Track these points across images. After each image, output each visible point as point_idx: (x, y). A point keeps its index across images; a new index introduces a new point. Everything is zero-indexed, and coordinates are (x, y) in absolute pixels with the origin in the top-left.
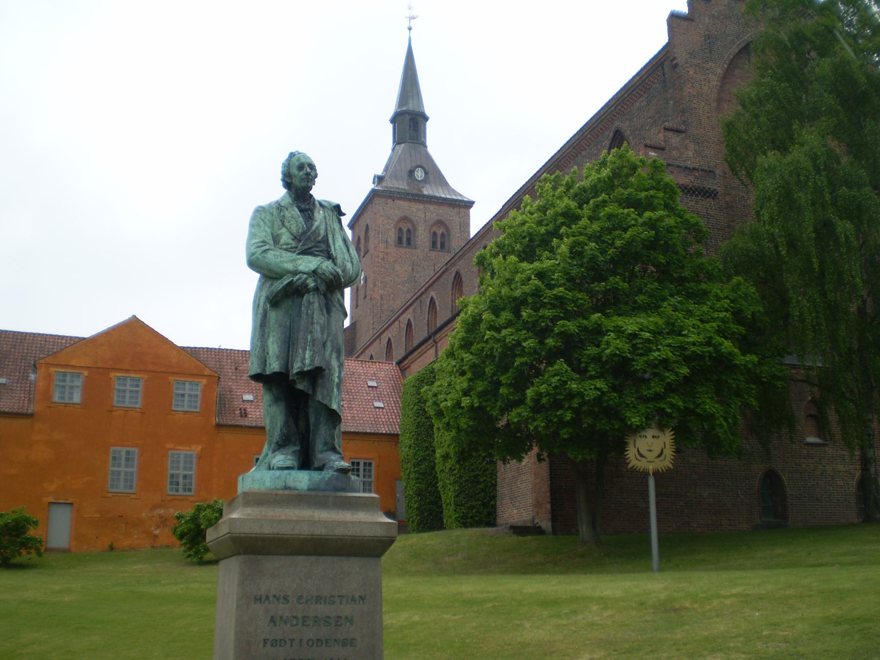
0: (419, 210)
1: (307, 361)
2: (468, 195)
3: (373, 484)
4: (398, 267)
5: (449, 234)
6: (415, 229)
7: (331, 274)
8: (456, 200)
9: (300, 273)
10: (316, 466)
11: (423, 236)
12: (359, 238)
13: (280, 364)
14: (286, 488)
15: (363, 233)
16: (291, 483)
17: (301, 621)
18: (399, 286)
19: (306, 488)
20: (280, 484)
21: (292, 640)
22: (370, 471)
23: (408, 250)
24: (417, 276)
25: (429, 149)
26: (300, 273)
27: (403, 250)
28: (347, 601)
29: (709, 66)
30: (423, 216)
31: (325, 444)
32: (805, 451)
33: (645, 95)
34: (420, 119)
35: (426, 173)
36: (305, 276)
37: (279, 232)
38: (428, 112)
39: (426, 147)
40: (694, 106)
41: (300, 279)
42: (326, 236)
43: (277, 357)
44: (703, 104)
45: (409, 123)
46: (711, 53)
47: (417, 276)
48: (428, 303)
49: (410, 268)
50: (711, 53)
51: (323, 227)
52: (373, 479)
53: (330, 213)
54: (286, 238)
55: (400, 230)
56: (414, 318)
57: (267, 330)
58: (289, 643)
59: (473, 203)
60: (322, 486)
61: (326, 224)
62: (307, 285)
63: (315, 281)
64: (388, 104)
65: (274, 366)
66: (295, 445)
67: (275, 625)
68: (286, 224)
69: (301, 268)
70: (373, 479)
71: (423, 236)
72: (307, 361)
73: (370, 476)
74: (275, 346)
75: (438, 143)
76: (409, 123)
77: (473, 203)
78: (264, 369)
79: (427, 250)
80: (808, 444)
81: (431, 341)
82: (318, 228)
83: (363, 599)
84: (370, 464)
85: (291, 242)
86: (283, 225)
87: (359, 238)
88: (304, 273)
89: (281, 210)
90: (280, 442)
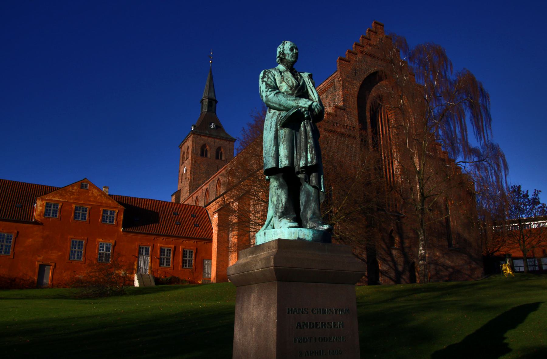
1: (309, 160)
4: (201, 166)
74: (286, 151)
84: (192, 252)
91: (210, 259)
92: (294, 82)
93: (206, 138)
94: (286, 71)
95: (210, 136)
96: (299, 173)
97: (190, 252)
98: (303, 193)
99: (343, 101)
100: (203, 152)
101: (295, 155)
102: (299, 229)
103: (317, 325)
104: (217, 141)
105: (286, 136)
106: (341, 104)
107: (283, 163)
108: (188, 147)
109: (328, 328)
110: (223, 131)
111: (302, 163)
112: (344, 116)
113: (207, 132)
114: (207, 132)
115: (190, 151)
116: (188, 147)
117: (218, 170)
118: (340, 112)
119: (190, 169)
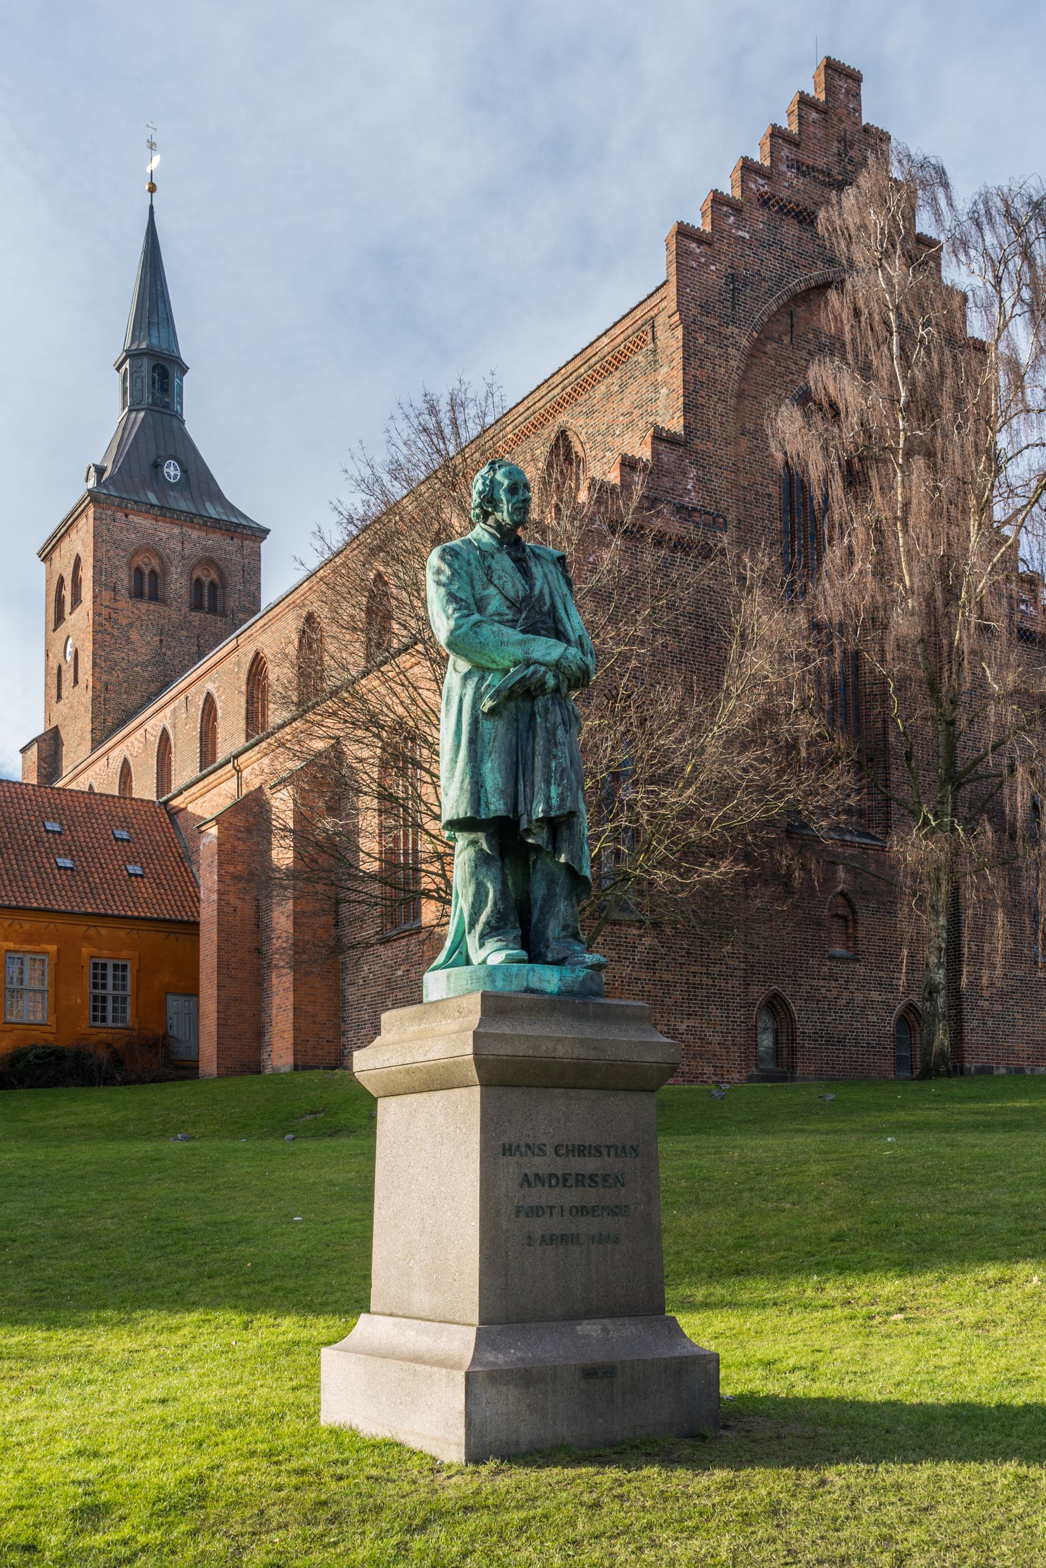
0: (171, 536)
1: (554, 802)
2: (257, 515)
3: (129, 1000)
4: (134, 636)
5: (224, 587)
6: (165, 571)
7: (579, 668)
8: (238, 525)
9: (533, 663)
10: (550, 957)
11: (177, 584)
12: (61, 580)
13: (505, 804)
14: (529, 990)
15: (70, 570)
16: (535, 984)
17: (561, 1179)
18: (138, 669)
19: (556, 990)
20: (516, 985)
21: (551, 1208)
22: (124, 978)
23: (152, 607)
24: (169, 653)
25: (187, 426)
26: (535, 662)
27: (144, 606)
28: (616, 1152)
29: (728, 331)
30: (179, 548)
31: (565, 927)
32: (825, 969)
33: (617, 374)
34: (174, 372)
35: (184, 471)
36: (543, 668)
37: (486, 592)
38: (186, 354)
39: (183, 422)
40: (701, 401)
41: (535, 672)
42: (553, 605)
43: (502, 792)
44: (715, 398)
45: (155, 371)
46: (734, 308)
47: (169, 653)
48: (201, 703)
49: (157, 638)
50: (734, 308)
51: (546, 591)
52: (129, 992)
53: (552, 567)
54: (496, 603)
55: (139, 571)
56: (174, 726)
57: (479, 750)
58: (547, 1211)
59: (267, 531)
60: (576, 988)
61: (549, 587)
62: (545, 683)
63: (556, 677)
64: (115, 331)
65: (496, 806)
66: (514, 928)
67: (530, 1186)
68: (496, 582)
69: (536, 655)
70: (129, 992)
71: (177, 584)
72: (554, 802)
73: (124, 988)
74: (497, 775)
75: (207, 414)
76: (155, 371)
77: (267, 531)
78: (478, 812)
79: (185, 609)
80: (832, 958)
81: (230, 766)
82: (541, 593)
83: (635, 1151)
84: (124, 967)
85: (507, 611)
86: (490, 581)
87: (61, 580)
88: (542, 664)
89: (484, 558)
90: (493, 922)
91: (193, 992)
92: (521, 588)
93: (144, 523)
94: (499, 551)
95: (165, 513)
96: (528, 831)
97: (116, 967)
98: (539, 876)
99: (687, 408)
100: (147, 586)
101: (521, 788)
102: (528, 966)
103: (565, 1180)
104: (195, 534)
105: (499, 738)
106: (676, 425)
107: (492, 807)
108: (78, 560)
109: (590, 1186)
110: (216, 495)
111: (539, 811)
112: (684, 474)
113: (152, 498)
114: (152, 498)
115: (87, 574)
116: (78, 560)
117: (201, 655)
118: (669, 457)
119: (89, 646)
